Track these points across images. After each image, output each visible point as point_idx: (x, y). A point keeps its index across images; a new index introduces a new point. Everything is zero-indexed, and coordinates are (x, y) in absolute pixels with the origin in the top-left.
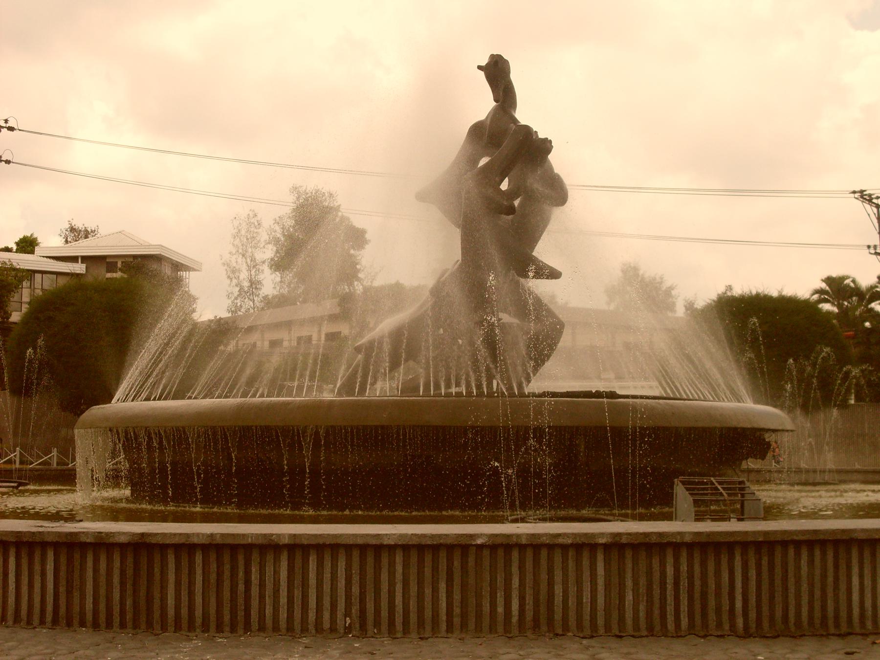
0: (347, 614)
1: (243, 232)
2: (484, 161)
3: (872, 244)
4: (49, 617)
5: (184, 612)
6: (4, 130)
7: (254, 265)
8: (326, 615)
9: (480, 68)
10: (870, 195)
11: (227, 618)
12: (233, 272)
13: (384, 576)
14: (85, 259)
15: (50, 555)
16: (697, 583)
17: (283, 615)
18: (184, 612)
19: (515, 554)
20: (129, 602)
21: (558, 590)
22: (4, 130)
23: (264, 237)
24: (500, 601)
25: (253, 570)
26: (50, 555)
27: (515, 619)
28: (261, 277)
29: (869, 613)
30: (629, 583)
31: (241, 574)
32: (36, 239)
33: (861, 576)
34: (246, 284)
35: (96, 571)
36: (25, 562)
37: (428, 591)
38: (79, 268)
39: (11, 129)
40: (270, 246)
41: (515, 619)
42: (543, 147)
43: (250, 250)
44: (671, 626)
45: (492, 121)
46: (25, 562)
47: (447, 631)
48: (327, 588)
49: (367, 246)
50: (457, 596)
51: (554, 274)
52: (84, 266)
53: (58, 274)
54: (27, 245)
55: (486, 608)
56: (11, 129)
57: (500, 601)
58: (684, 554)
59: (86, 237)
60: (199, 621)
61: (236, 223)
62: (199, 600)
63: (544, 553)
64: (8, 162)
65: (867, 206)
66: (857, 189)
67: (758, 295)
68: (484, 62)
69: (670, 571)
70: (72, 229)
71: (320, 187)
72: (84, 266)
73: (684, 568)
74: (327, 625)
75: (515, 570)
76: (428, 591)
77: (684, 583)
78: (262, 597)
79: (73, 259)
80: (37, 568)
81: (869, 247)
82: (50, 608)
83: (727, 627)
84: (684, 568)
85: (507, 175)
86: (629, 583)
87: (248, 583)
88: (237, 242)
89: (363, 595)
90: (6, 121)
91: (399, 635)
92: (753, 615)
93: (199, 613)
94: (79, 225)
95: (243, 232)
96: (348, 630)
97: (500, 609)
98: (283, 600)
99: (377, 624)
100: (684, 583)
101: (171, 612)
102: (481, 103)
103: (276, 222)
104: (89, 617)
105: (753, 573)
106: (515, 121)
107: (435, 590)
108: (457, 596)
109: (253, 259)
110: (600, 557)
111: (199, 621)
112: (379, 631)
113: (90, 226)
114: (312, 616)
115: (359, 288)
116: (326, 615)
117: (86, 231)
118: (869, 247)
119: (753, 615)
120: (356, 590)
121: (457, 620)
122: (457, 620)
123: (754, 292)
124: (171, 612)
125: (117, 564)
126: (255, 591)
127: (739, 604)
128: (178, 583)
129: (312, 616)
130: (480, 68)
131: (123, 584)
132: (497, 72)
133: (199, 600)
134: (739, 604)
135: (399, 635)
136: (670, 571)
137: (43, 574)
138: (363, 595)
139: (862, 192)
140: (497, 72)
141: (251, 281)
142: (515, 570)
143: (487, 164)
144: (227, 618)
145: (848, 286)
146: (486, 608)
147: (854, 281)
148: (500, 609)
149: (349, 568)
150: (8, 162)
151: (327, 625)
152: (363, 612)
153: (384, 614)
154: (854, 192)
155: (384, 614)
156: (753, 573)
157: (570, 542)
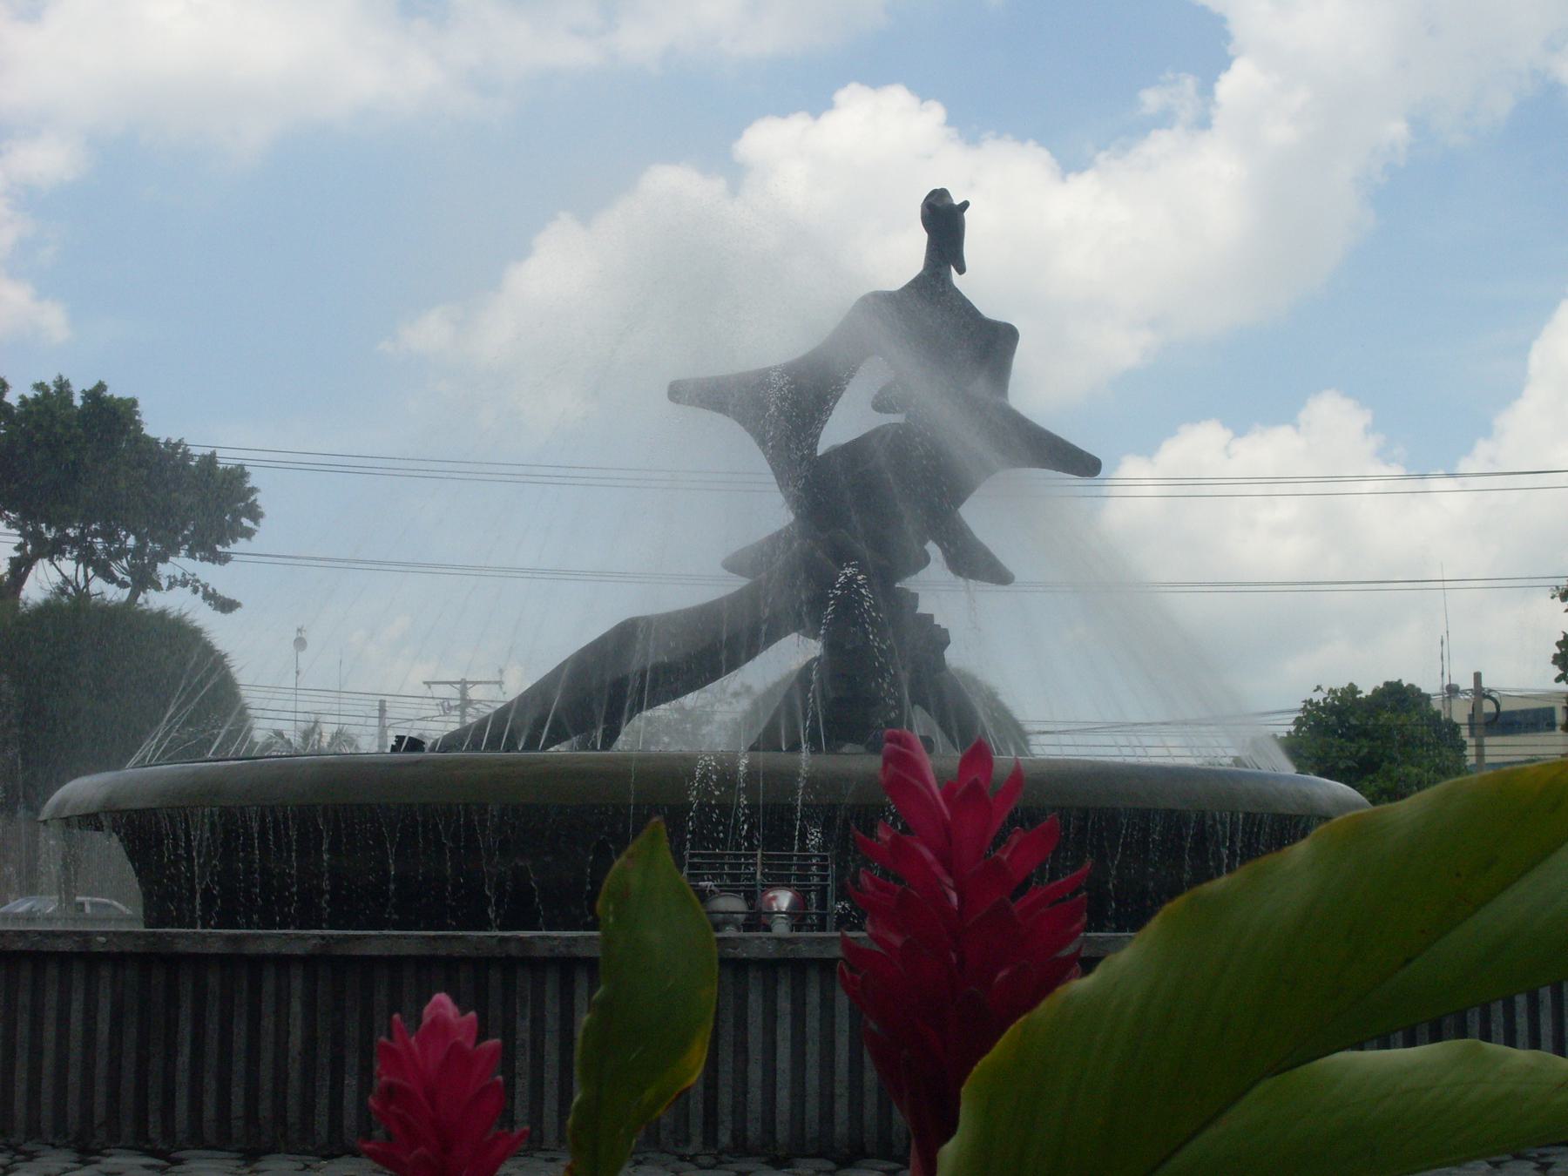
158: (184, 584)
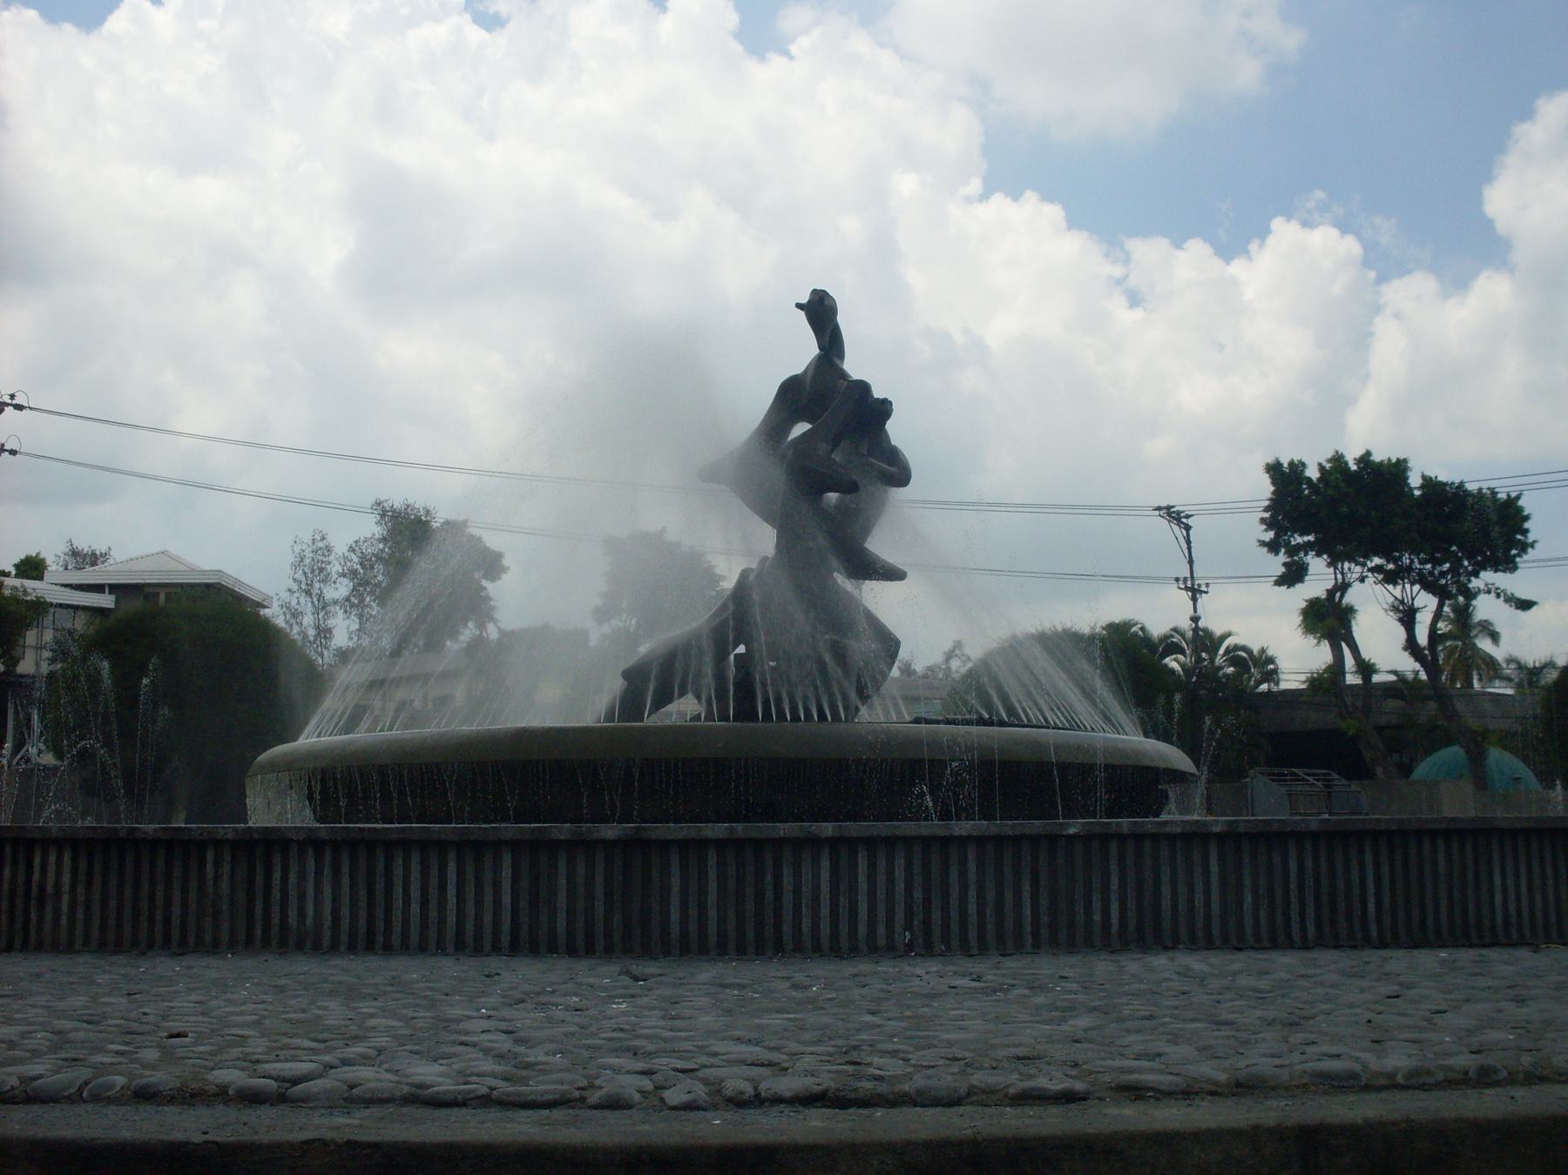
0: (908, 927)
1: (307, 561)
2: (801, 428)
3: (1181, 576)
4: (505, 939)
5: (693, 928)
6: (9, 410)
7: (322, 606)
8: (881, 929)
9: (799, 306)
10: (1178, 513)
11: (751, 936)
12: (294, 615)
13: (954, 876)
14: (114, 588)
15: (507, 859)
16: (1324, 883)
17: (825, 929)
18: (693, 928)
19: (1114, 848)
20: (617, 918)
21: (1166, 891)
22: (9, 410)
23: (335, 568)
24: (1097, 905)
25: (785, 872)
26: (507, 859)
27: (1114, 929)
28: (331, 622)
29: (1514, 919)
30: (1247, 882)
31: (769, 878)
32: (43, 560)
33: (1503, 873)
34: (311, 632)
35: (571, 877)
36: (470, 870)
37: (1009, 895)
38: (106, 601)
39: (19, 407)
40: (345, 581)
41: (1114, 929)
42: (883, 409)
43: (317, 585)
44: (1296, 936)
45: (814, 378)
46: (470, 870)
47: (1033, 946)
48: (881, 894)
49: (504, 576)
50: (1044, 902)
51: (892, 574)
52: (113, 598)
53: (76, 608)
54: (32, 567)
55: (1080, 918)
56: (19, 407)
57: (1097, 905)
58: (1308, 846)
59: (94, 564)
60: (713, 939)
61: (297, 549)
62: (712, 914)
63: (1148, 846)
64: (13, 452)
65: (1176, 528)
66: (1163, 504)
67: (1065, 631)
68: (805, 300)
69: (1293, 866)
70: (75, 553)
71: (410, 501)
72: (113, 598)
73: (1309, 863)
74: (881, 941)
75: (1114, 867)
76: (1009, 895)
77: (1309, 883)
78: (797, 908)
79: (98, 588)
80: (488, 876)
81: (1177, 580)
82: (506, 927)
83: (1359, 935)
84: (1309, 863)
85: (830, 442)
86: (1247, 882)
87: (778, 888)
88: (299, 575)
89: (927, 901)
90: (12, 397)
91: (974, 951)
92: (1387, 921)
93: (712, 930)
94: (83, 545)
95: (307, 561)
96: (909, 947)
97: (1097, 917)
98: (825, 911)
99: (946, 940)
100: (1309, 883)
101: (675, 928)
102: (802, 350)
103: (352, 550)
104: (562, 940)
105: (1385, 869)
106: (843, 375)
107: (1018, 895)
108: (1044, 902)
109: (320, 596)
110: (1213, 850)
111: (713, 939)
112: (948, 947)
113: (100, 548)
114: (862, 929)
115: (492, 632)
116: (881, 929)
117: (94, 554)
118: (1177, 580)
119: (1387, 921)
120: (918, 894)
121: (1044, 932)
122: (1044, 932)
123: (1060, 629)
124: (675, 928)
125: (600, 868)
126: (787, 898)
127: (1371, 907)
128: (684, 891)
129: (862, 929)
130: (799, 306)
131: (608, 894)
132: (820, 311)
133: (712, 914)
134: (1371, 907)
135: (974, 951)
136: (1293, 866)
137: (497, 884)
138: (927, 901)
139: (1169, 508)
140: (820, 311)
141: (317, 627)
142: (1114, 867)
143: (804, 435)
144: (751, 936)
145: (1135, 634)
146: (1080, 918)
147: (1142, 629)
148: (1097, 917)
149: (909, 867)
150: (13, 452)
151: (881, 941)
152: (927, 923)
153: (954, 926)
154: (1159, 509)
155: (954, 926)
156: (1385, 869)
157: (1179, 830)
158: (1489, 592)
